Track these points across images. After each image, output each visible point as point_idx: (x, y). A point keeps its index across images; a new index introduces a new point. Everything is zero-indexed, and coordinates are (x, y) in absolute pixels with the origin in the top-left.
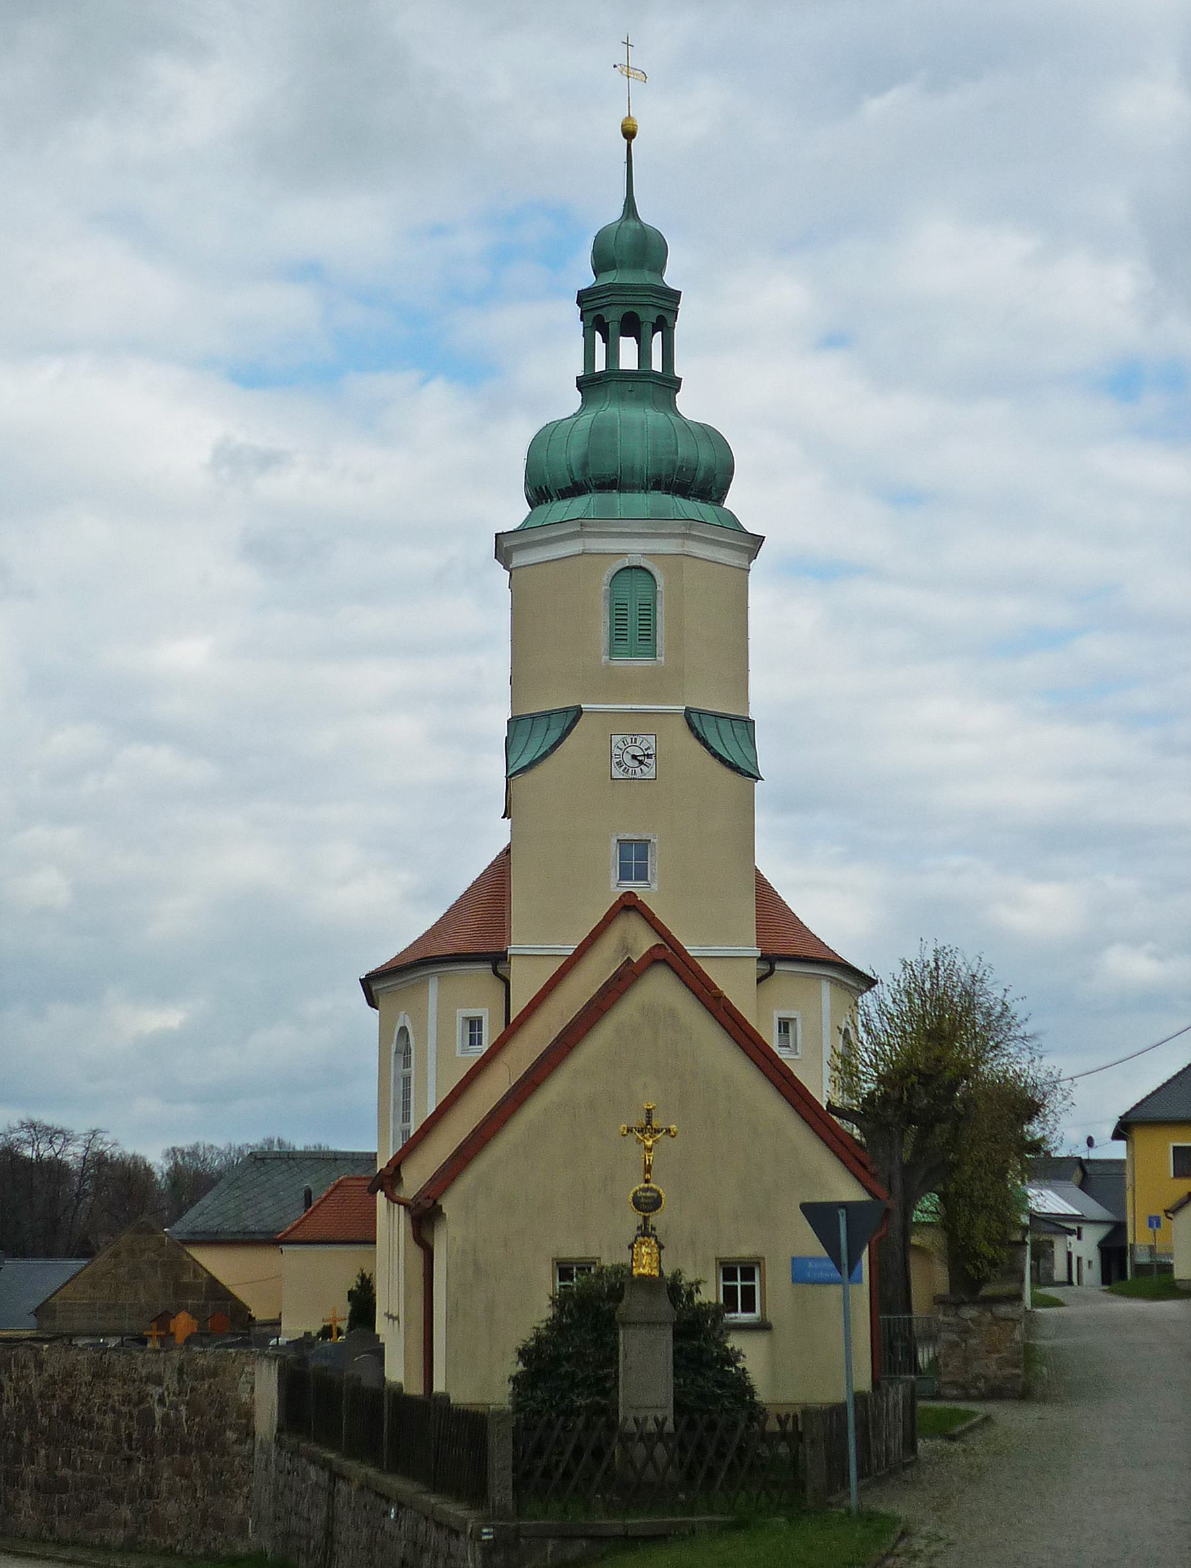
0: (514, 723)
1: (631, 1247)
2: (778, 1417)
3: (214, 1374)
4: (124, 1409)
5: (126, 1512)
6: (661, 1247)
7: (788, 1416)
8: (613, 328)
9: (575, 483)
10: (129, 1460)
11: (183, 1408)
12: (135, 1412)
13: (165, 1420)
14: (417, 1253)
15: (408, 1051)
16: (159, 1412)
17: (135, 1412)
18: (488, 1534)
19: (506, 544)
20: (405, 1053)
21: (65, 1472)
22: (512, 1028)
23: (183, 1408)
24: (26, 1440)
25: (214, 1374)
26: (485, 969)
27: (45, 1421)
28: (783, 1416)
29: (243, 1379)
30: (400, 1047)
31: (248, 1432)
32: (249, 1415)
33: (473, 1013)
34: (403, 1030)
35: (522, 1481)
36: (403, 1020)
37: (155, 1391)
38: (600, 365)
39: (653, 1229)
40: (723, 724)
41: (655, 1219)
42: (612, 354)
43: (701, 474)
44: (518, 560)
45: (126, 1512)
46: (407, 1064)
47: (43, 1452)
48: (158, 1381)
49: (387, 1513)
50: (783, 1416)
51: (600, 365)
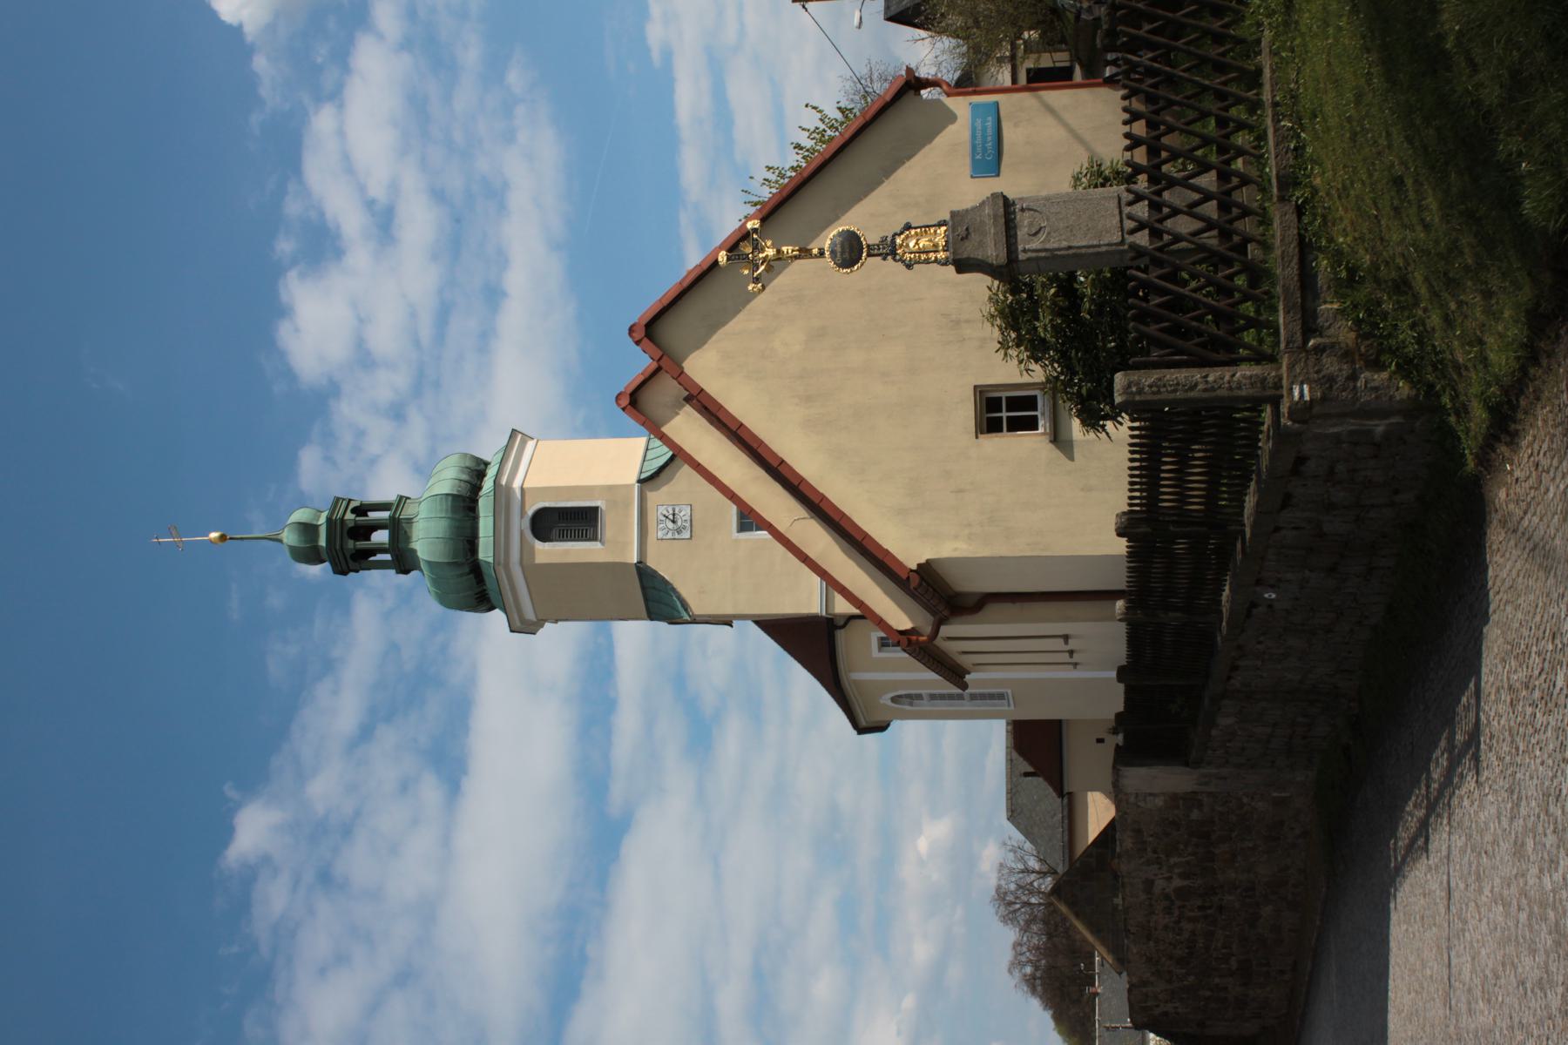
0: (652, 615)
1: (909, 266)
2: (1128, 149)
3: (1139, 831)
4: (1177, 913)
5: (1267, 910)
6: (908, 227)
7: (1125, 110)
8: (362, 544)
9: (471, 572)
10: (1221, 909)
11: (1173, 860)
12: (1178, 903)
13: (1184, 876)
14: (992, 609)
15: (909, 696)
16: (1177, 882)
17: (1178, 903)
18: (1302, 395)
19: (518, 624)
20: (912, 698)
21: (1234, 964)
22: (749, 519)
23: (1173, 860)
24: (1208, 993)
25: (1139, 831)
26: (840, 635)
27: (1191, 978)
28: (1128, 142)
29: (1142, 804)
30: (909, 703)
31: (1191, 800)
32: (1174, 798)
33: (875, 644)
34: (894, 700)
35: (1221, 351)
36: (886, 699)
37: (1160, 884)
38: (388, 557)
39: (884, 239)
40: (650, 455)
41: (870, 237)
42: (380, 549)
43: (465, 477)
44: (530, 615)
45: (1267, 910)
46: (919, 697)
47: (1217, 980)
48: (1149, 884)
49: (1270, 605)
50: (1128, 142)
51: (388, 557)
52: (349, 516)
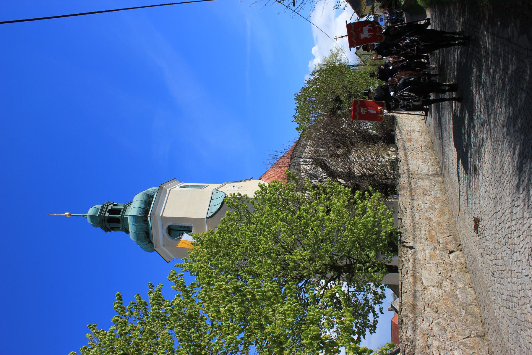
52: (107, 214)
